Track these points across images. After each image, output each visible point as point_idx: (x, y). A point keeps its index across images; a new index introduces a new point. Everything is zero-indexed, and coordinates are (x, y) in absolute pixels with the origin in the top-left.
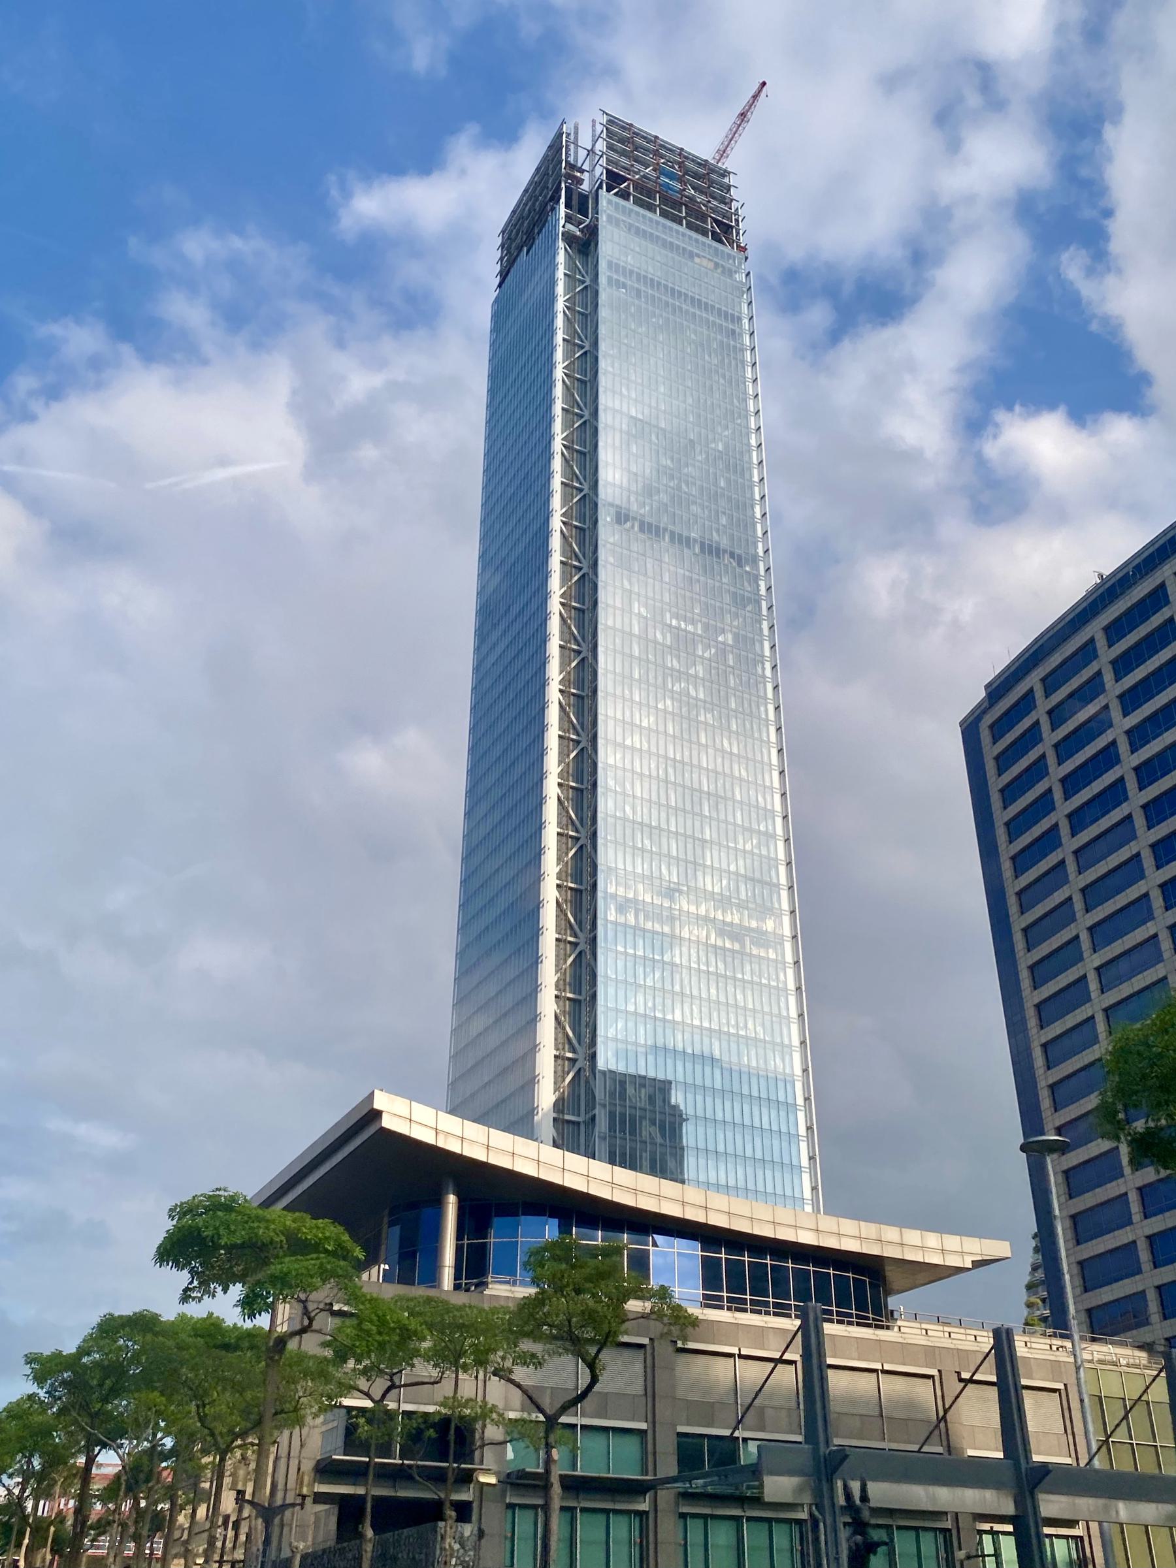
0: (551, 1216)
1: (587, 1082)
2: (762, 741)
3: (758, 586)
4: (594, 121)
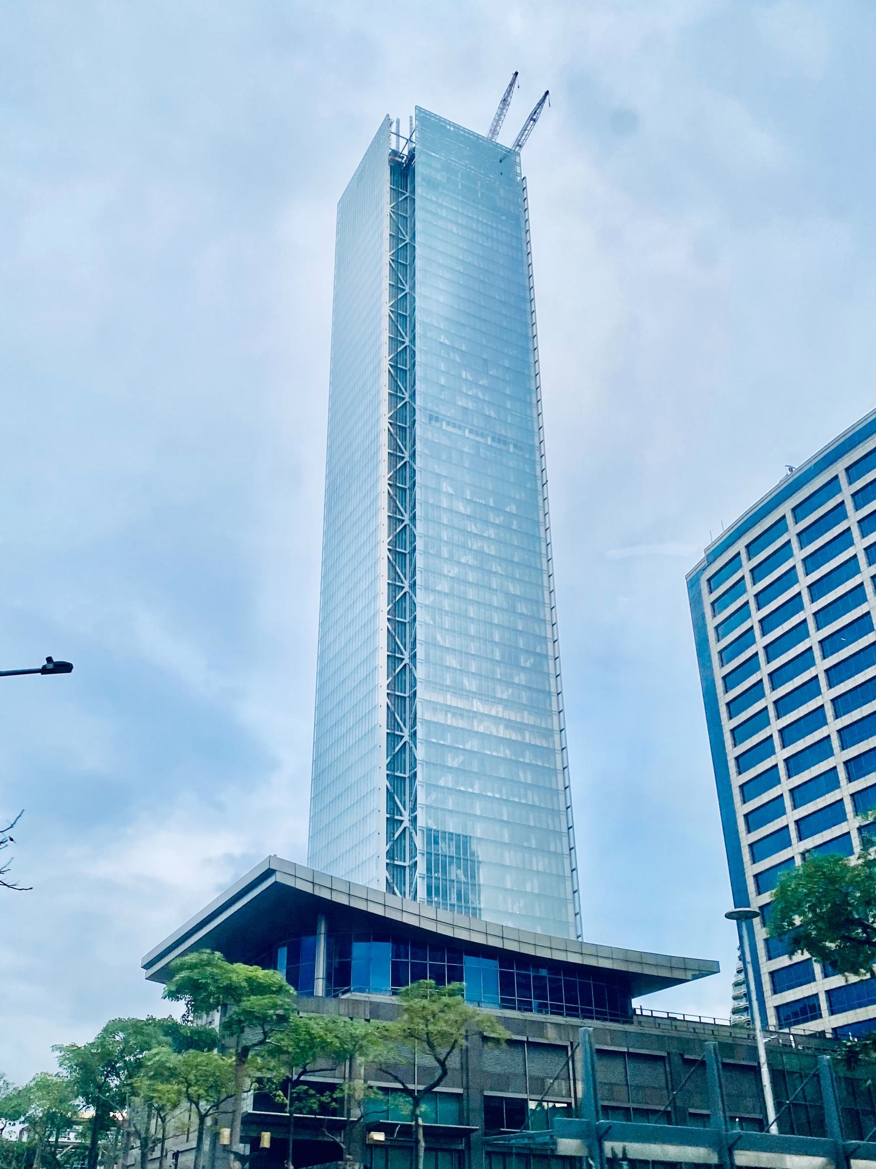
1: (411, 834)
3: (535, 468)
4: (411, 117)
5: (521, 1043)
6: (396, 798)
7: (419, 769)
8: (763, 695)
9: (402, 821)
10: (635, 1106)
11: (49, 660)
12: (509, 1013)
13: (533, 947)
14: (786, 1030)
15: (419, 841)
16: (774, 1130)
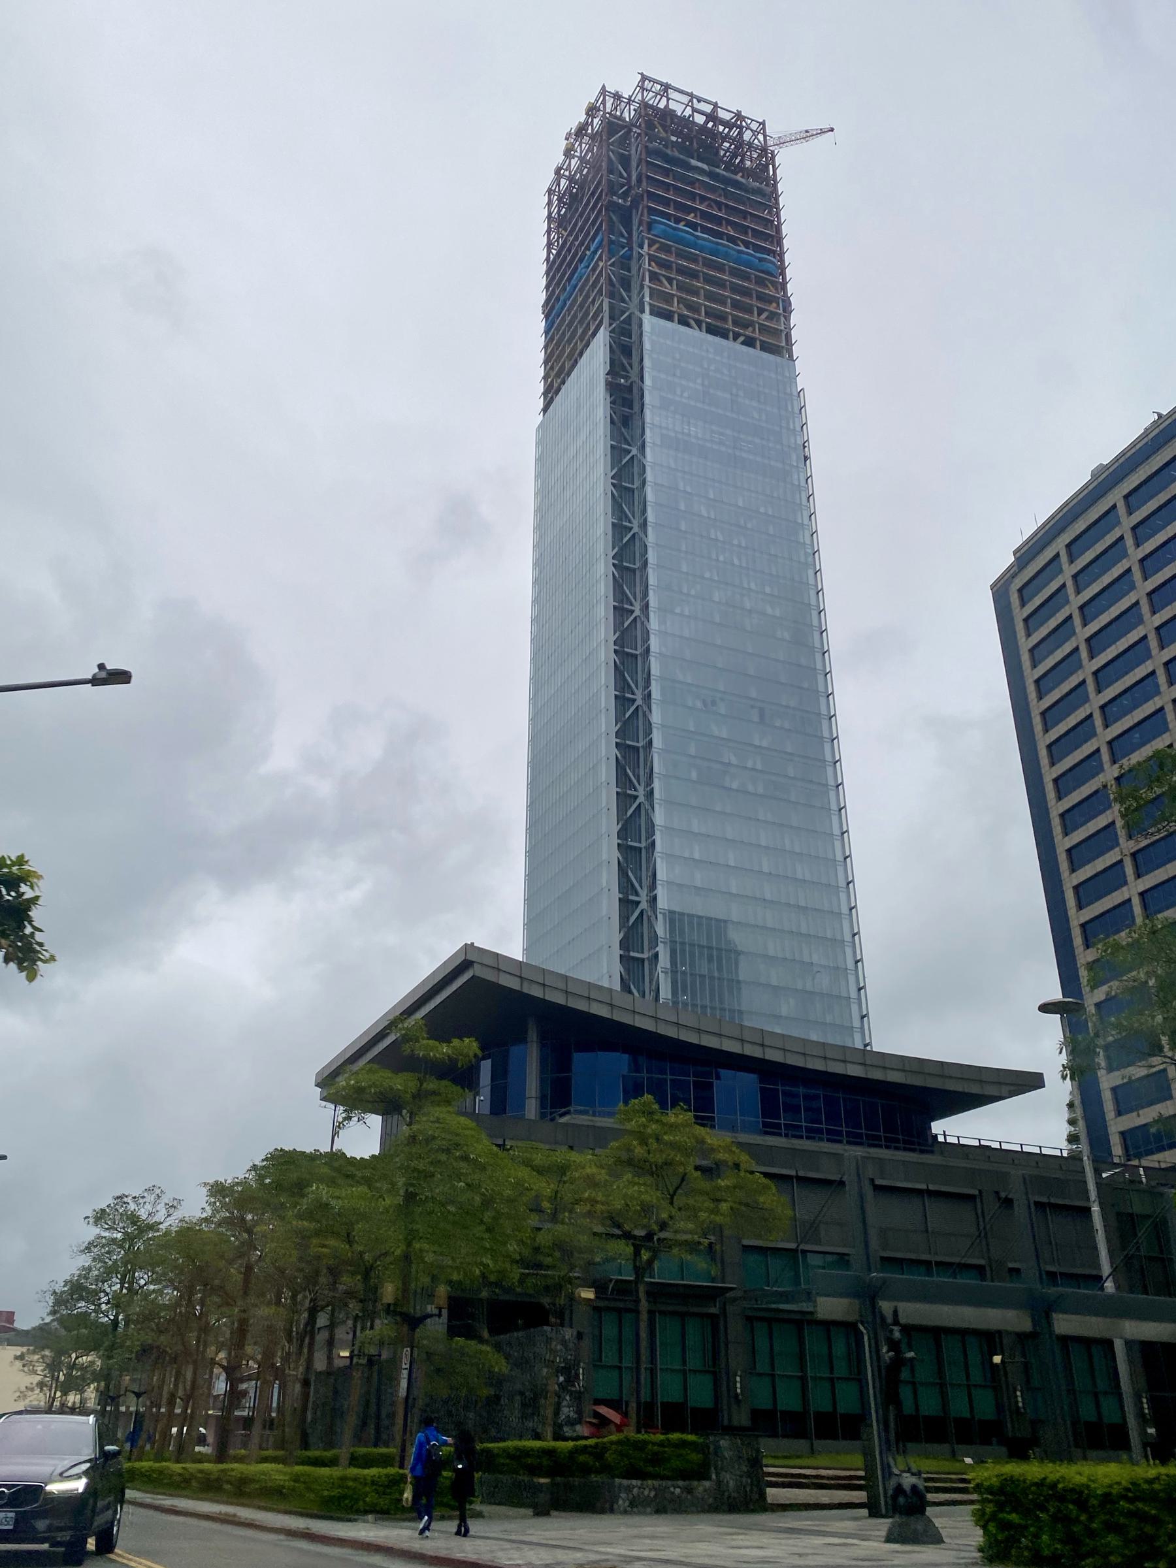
0: (624, 1052)
1: (646, 811)
2: (788, 429)
5: (789, 1177)
6: (630, 874)
7: (658, 837)
8: (1094, 734)
9: (638, 903)
10: (939, 1259)
11: (101, 667)
12: (772, 1141)
13: (781, 1052)
14: (1135, 1162)
15: (661, 929)
16: (1109, 1286)
